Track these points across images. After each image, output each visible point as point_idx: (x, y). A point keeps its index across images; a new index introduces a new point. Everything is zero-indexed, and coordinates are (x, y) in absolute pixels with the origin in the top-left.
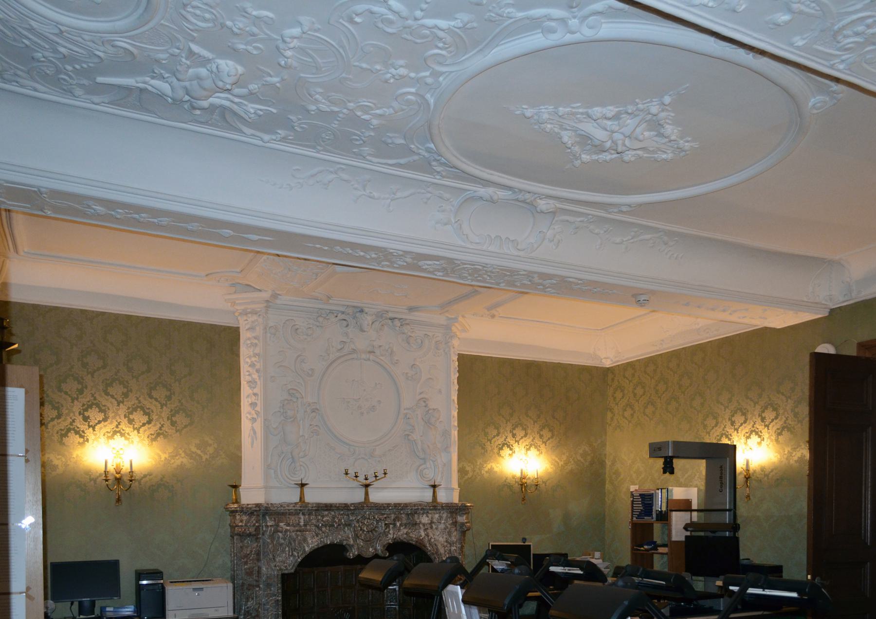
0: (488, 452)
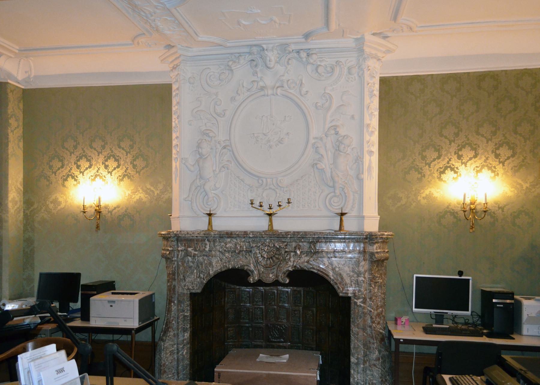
0: (427, 177)
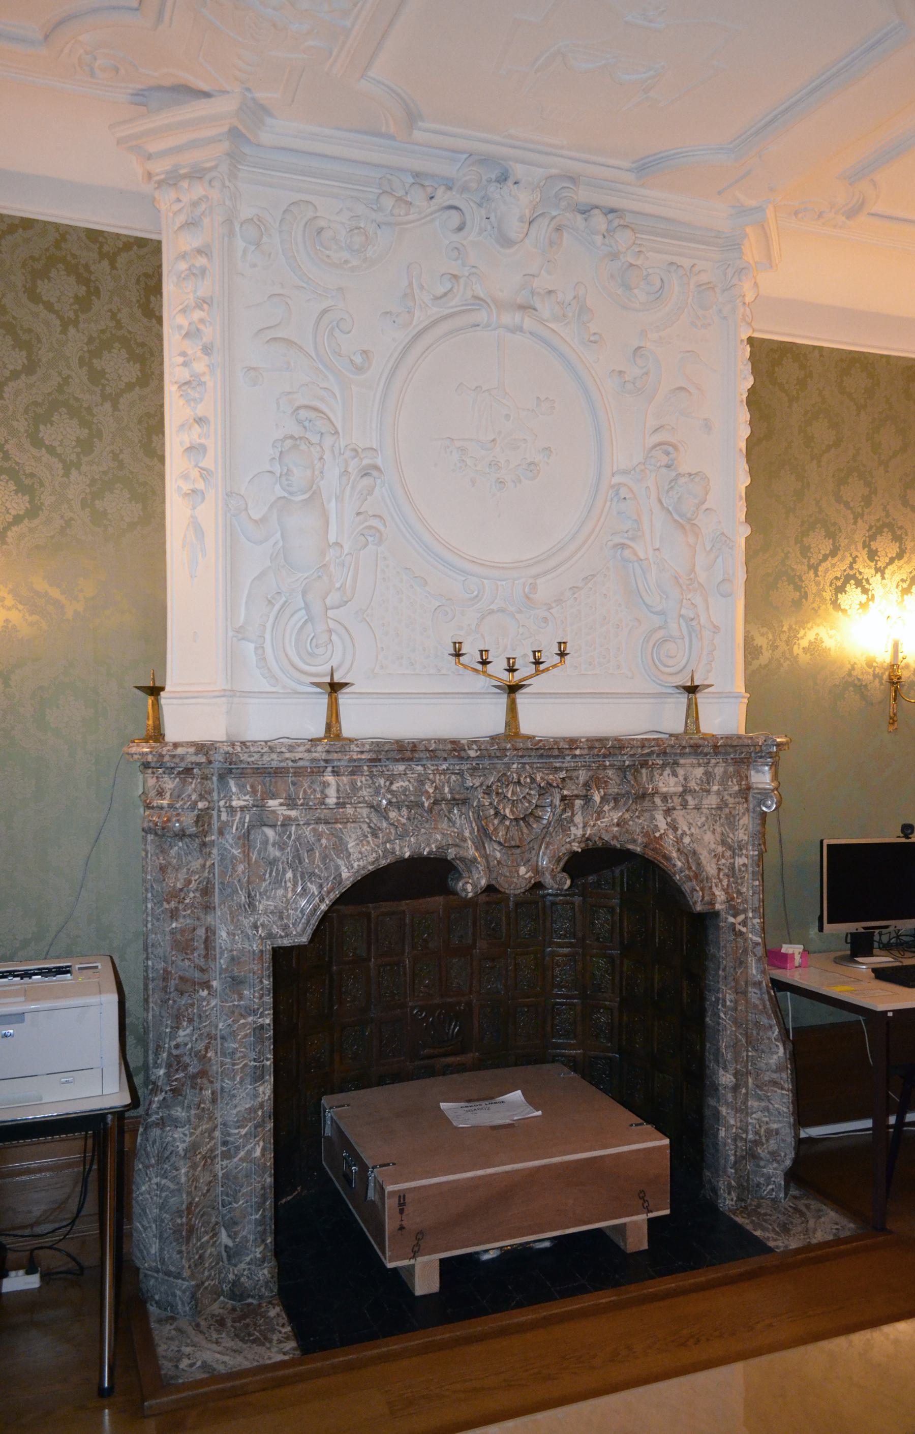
0: (811, 597)
